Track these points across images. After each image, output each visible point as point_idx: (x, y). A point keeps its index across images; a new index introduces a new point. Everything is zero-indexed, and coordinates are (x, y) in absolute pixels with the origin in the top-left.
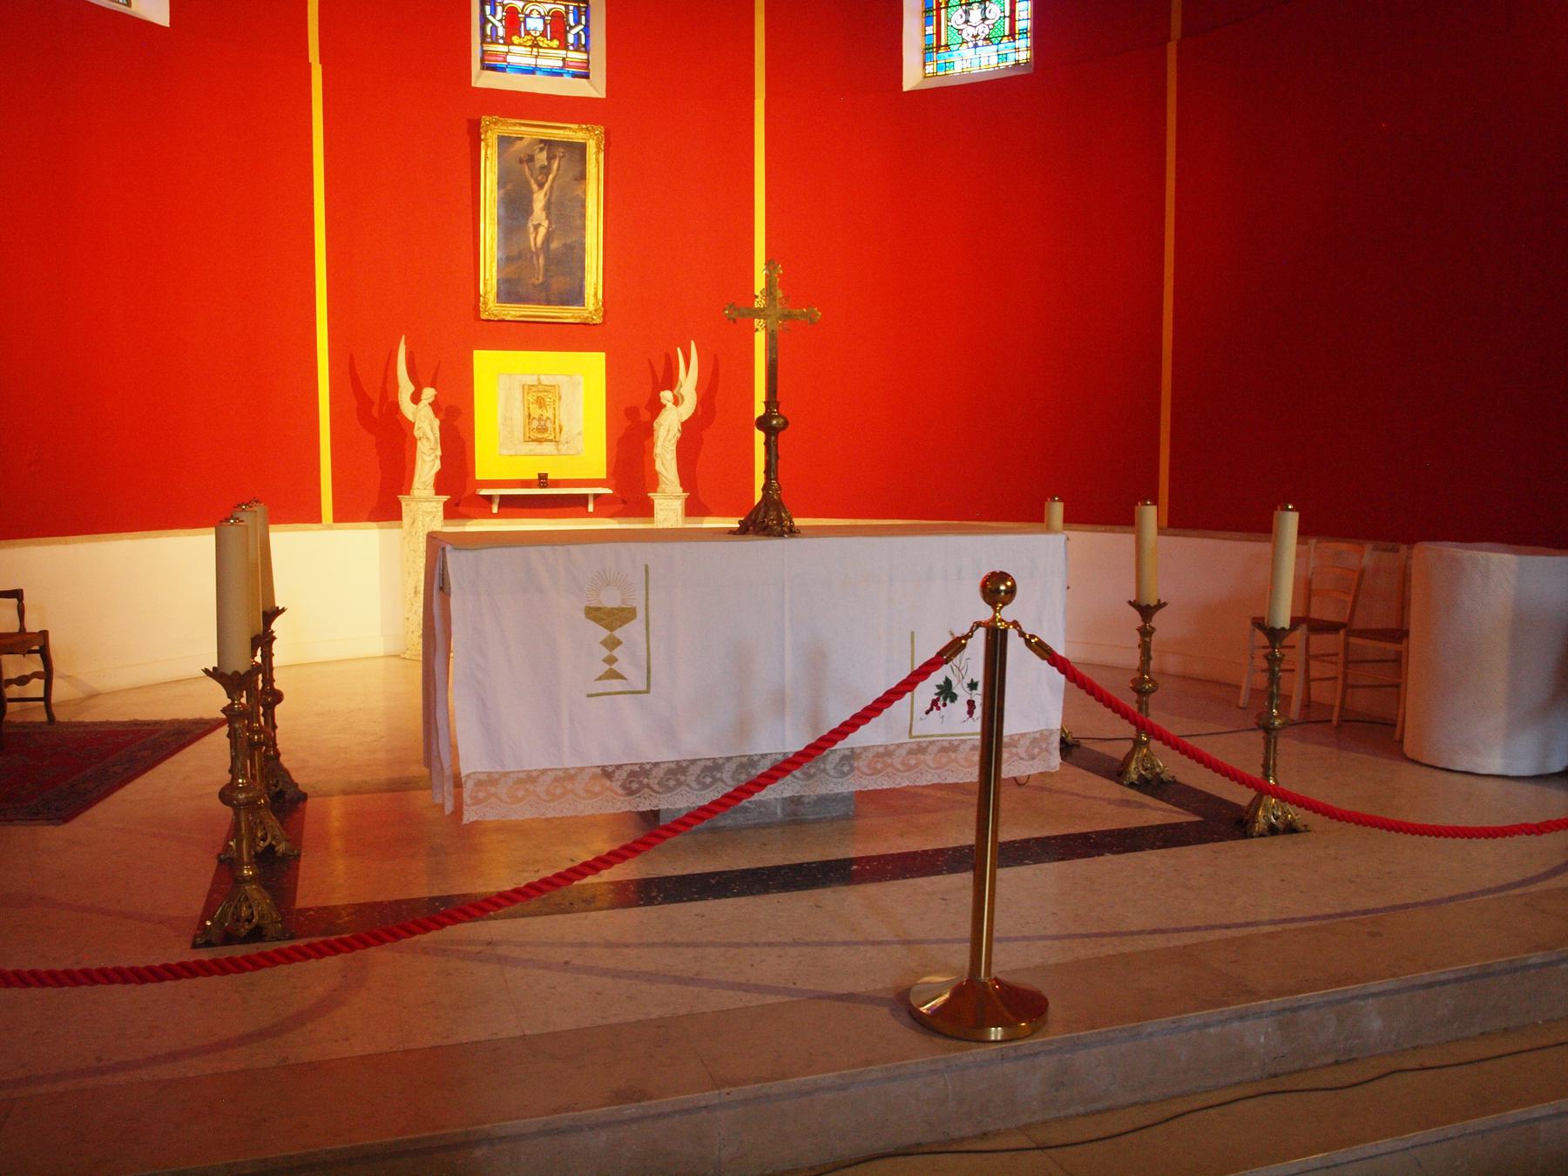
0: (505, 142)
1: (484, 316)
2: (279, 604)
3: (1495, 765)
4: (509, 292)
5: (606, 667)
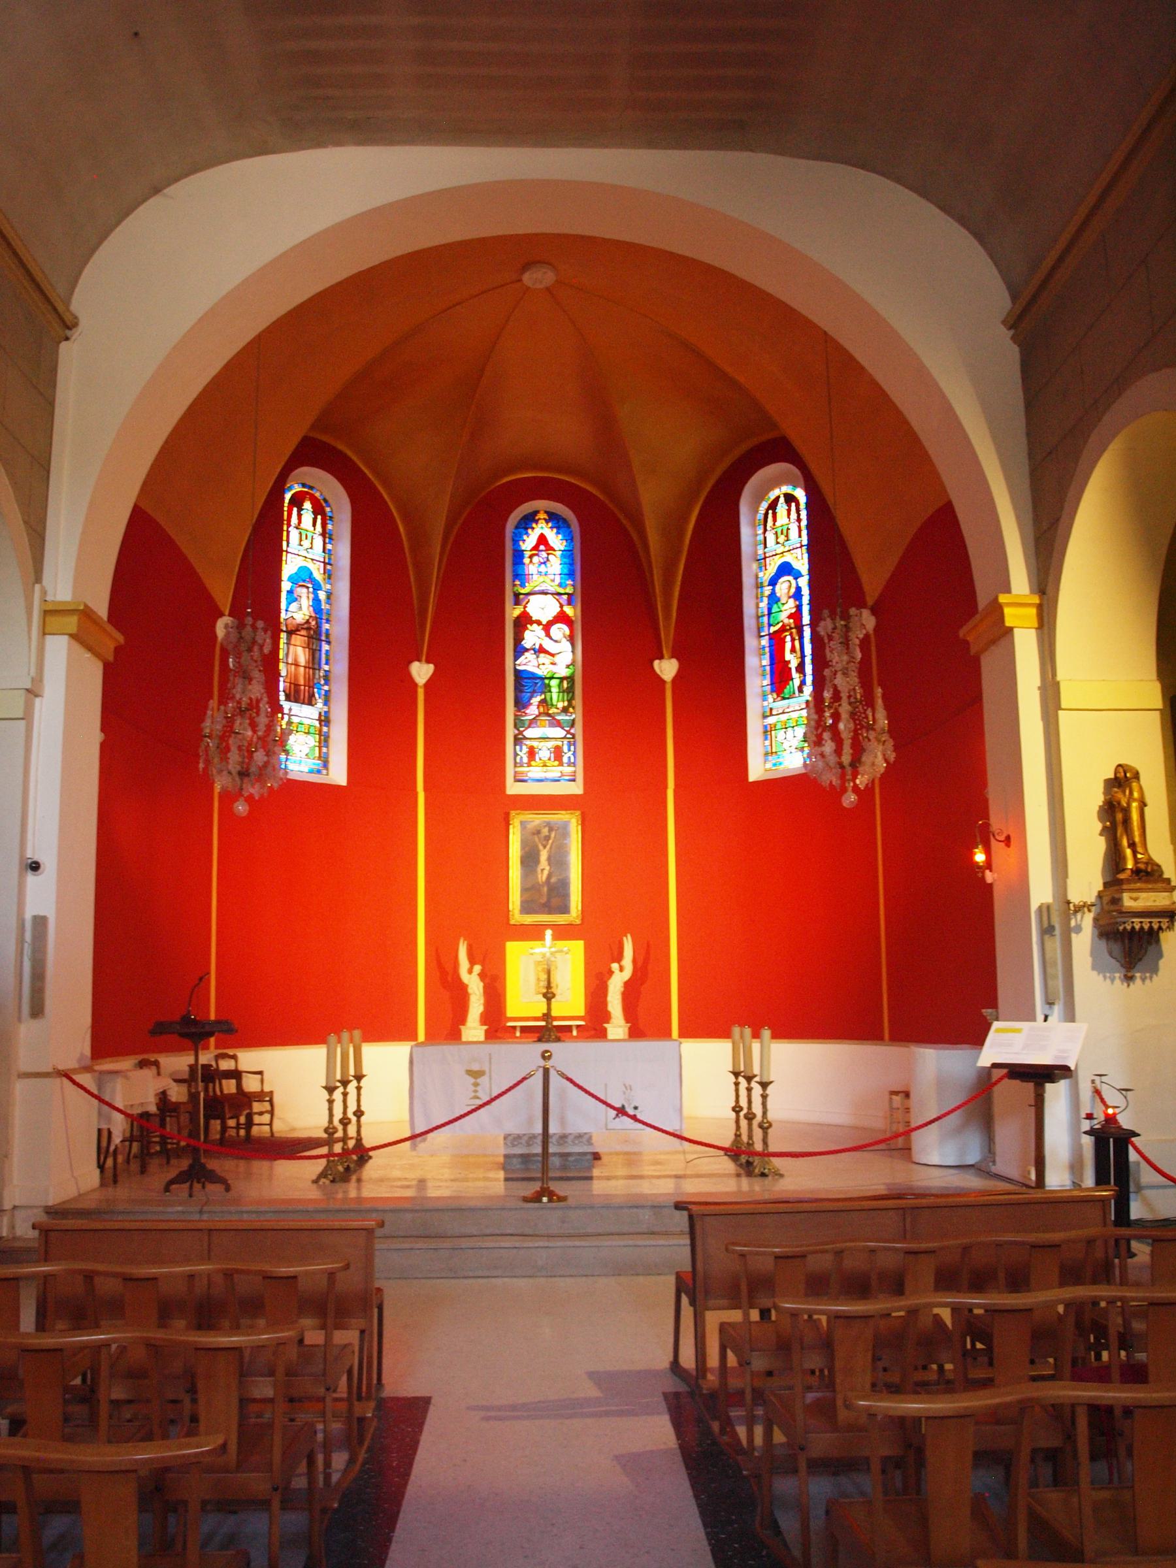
0: (522, 823)
1: (512, 922)
2: (364, 1073)
3: (935, 1160)
4: (526, 908)
5: (473, 1094)
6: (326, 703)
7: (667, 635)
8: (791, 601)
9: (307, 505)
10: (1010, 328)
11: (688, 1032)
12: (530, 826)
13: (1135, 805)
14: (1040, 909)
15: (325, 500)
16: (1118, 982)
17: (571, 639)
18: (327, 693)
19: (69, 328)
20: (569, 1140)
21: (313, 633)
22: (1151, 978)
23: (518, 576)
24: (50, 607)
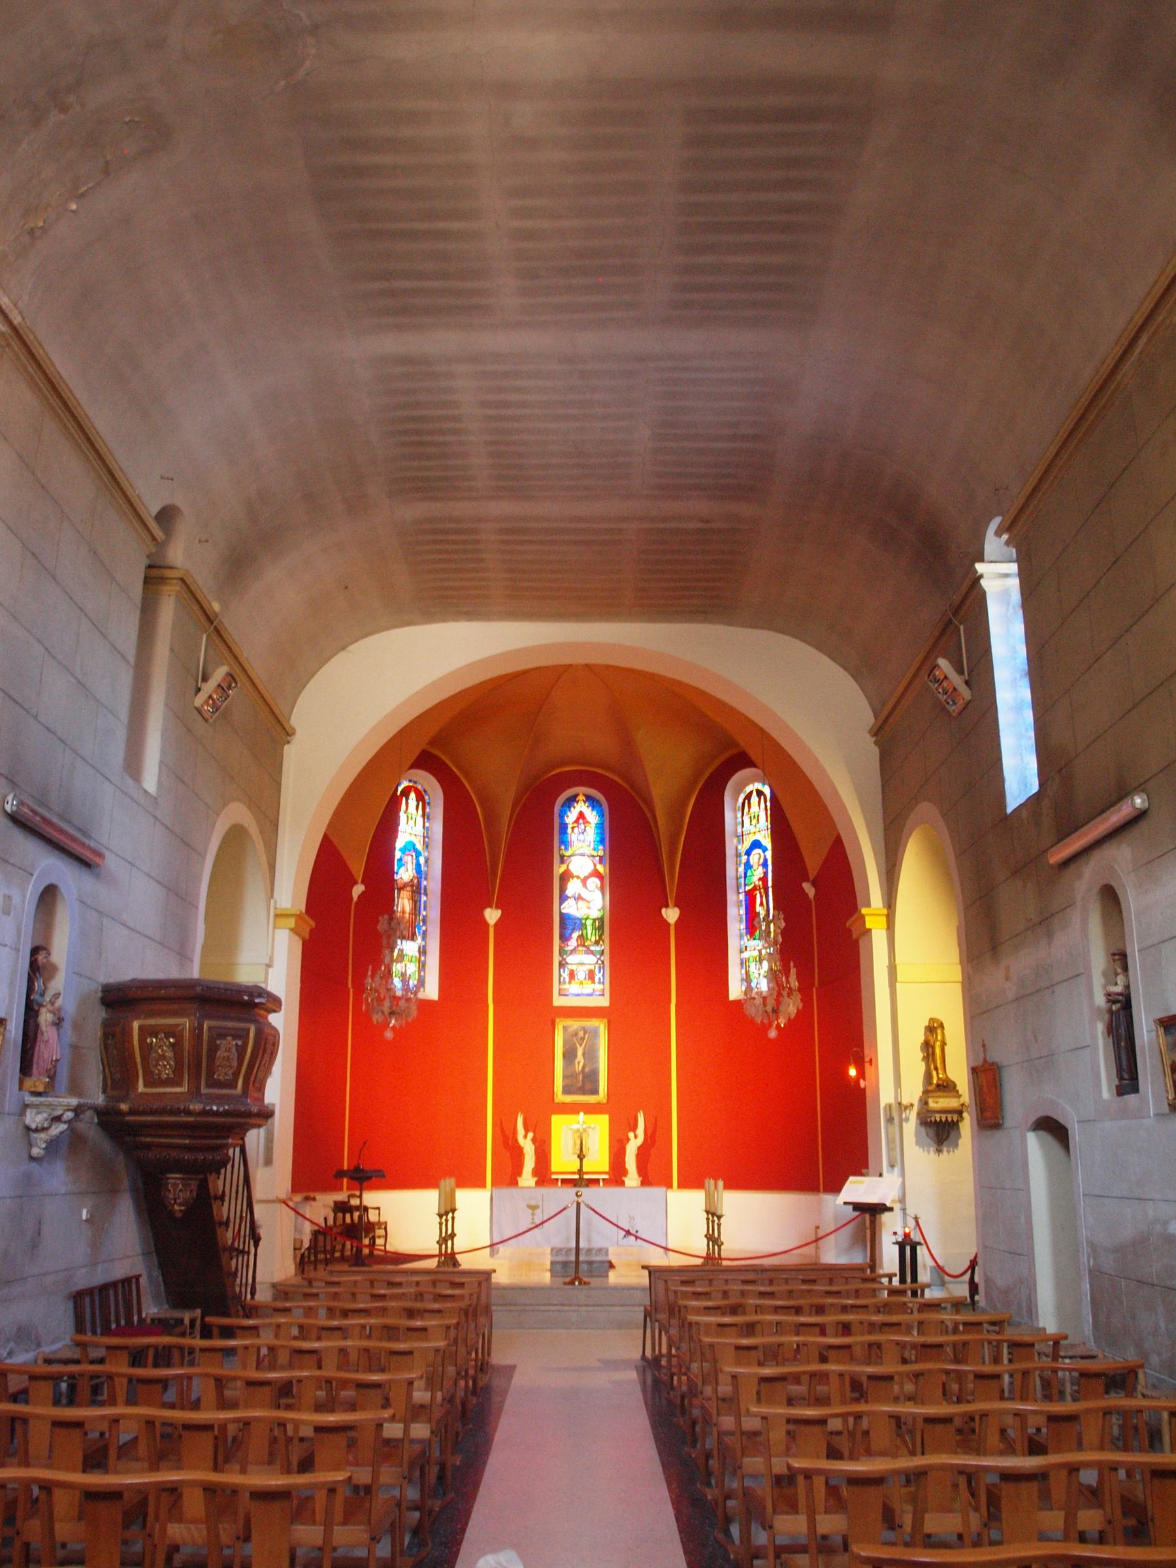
0: (565, 1028)
4: (567, 1090)
6: (424, 938)
7: (672, 891)
8: (761, 867)
9: (413, 795)
10: (873, 736)
11: (682, 1185)
12: (570, 1030)
13: (938, 1044)
14: (886, 1106)
15: (425, 791)
16: (932, 1153)
17: (602, 889)
18: (425, 933)
19: (288, 734)
20: (594, 1252)
21: (416, 889)
22: (953, 1151)
23: (564, 842)
24: (279, 912)
